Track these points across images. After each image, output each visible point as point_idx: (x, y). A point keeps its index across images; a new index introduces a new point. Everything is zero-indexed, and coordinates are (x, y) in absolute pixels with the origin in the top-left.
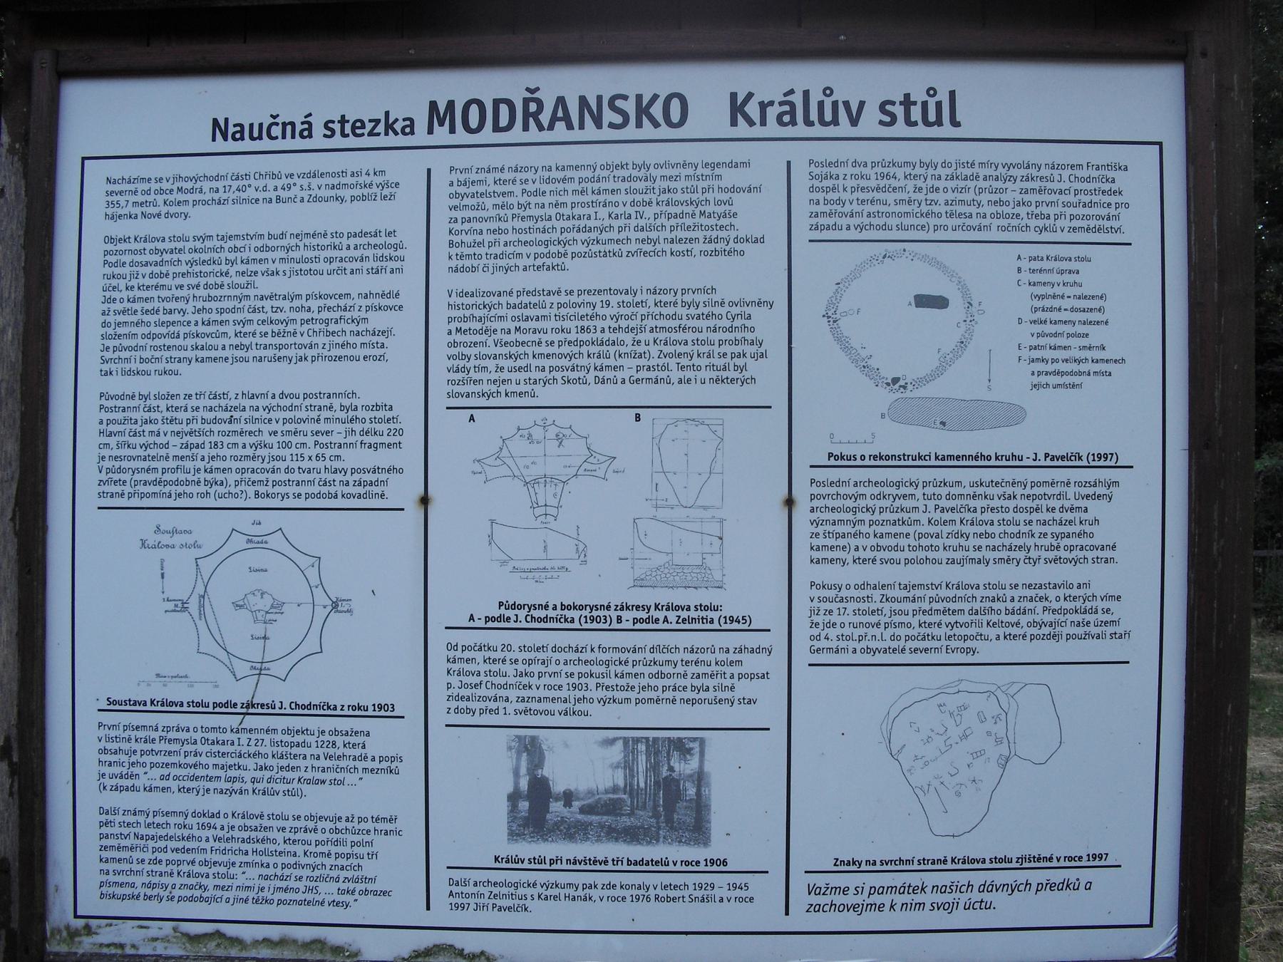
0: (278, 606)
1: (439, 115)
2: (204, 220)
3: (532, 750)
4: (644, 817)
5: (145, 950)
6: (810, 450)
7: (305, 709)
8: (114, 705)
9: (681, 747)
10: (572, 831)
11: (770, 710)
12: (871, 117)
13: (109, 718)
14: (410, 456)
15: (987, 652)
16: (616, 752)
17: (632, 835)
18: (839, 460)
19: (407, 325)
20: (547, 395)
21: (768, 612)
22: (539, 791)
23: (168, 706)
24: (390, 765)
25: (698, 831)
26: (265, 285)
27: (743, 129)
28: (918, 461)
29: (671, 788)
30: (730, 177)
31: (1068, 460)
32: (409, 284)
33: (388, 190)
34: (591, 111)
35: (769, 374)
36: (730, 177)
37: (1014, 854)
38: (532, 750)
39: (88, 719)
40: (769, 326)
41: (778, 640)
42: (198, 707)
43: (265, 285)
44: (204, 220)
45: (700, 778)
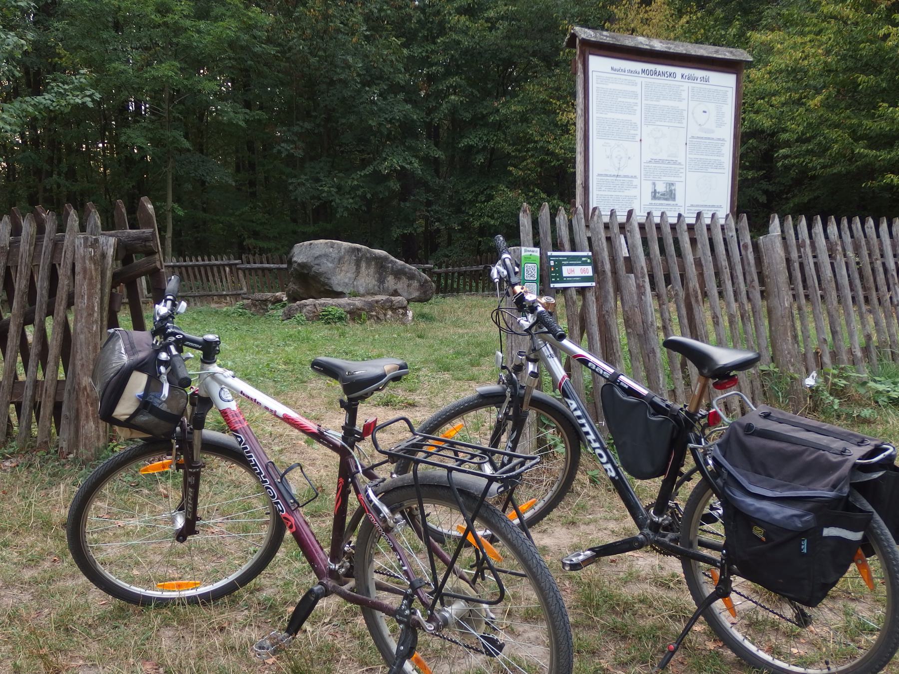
0: (621, 158)
1: (643, 71)
2: (611, 86)
3: (654, 184)
4: (668, 196)
5: (883, 590)
6: (689, 136)
7: (625, 176)
8: (599, 175)
9: (672, 184)
10: (659, 199)
11: (683, 179)
12: (699, 79)
13: (599, 177)
14: (638, 132)
15: (710, 170)
16: (665, 185)
17: (666, 199)
18: (693, 137)
19: (638, 108)
20: (658, 123)
21: (683, 163)
22: (655, 192)
23: (606, 175)
24: (636, 187)
25: (674, 199)
26: (620, 99)
27: (683, 80)
28: (702, 138)
29: (671, 191)
30: (681, 88)
31: (719, 139)
32: (639, 101)
33: (636, 84)
34: (664, 74)
35: (685, 121)
36: (681, 88)
37: (630, 175)
38: (654, 184)
39: (595, 177)
40: (685, 113)
41: (684, 167)
42: (610, 176)
43: (620, 99)
44: (611, 86)
45: (675, 190)
